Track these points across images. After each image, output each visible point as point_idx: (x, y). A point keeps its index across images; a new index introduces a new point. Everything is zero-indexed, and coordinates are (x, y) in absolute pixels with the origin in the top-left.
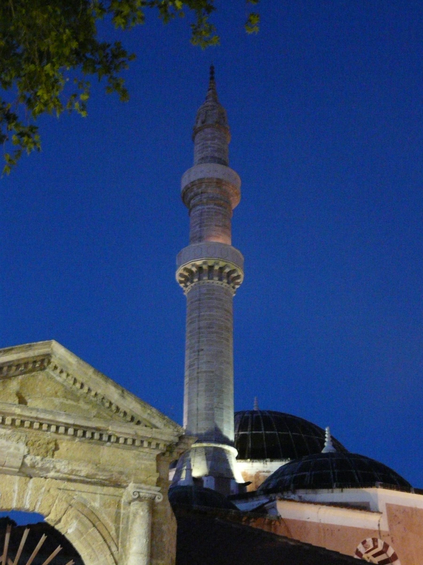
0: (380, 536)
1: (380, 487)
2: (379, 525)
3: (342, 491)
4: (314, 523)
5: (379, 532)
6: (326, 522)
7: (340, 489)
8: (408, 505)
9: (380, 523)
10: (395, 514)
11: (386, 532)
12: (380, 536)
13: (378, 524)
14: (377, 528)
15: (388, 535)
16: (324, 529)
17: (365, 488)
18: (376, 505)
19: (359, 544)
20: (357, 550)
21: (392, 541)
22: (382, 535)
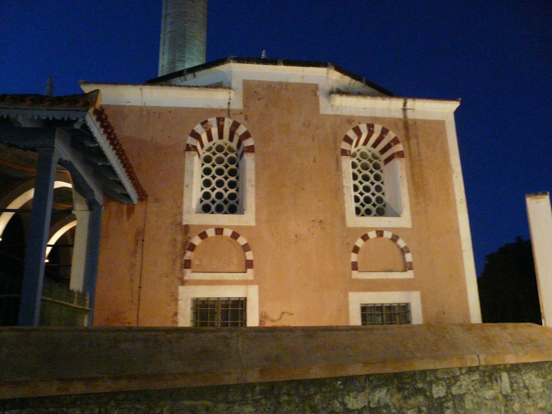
0: (229, 115)
1: (232, 61)
2: (229, 103)
3: (195, 76)
4: (136, 107)
5: (229, 111)
6: (153, 104)
7: (192, 74)
8: (277, 80)
9: (231, 101)
10: (251, 90)
11: (240, 110)
12: (229, 115)
13: (228, 102)
14: (226, 107)
15: (241, 113)
16: (148, 112)
17: (217, 66)
18: (230, 83)
19: (255, 142)
20: (193, 131)
21: (246, 119)
22: (231, 113)
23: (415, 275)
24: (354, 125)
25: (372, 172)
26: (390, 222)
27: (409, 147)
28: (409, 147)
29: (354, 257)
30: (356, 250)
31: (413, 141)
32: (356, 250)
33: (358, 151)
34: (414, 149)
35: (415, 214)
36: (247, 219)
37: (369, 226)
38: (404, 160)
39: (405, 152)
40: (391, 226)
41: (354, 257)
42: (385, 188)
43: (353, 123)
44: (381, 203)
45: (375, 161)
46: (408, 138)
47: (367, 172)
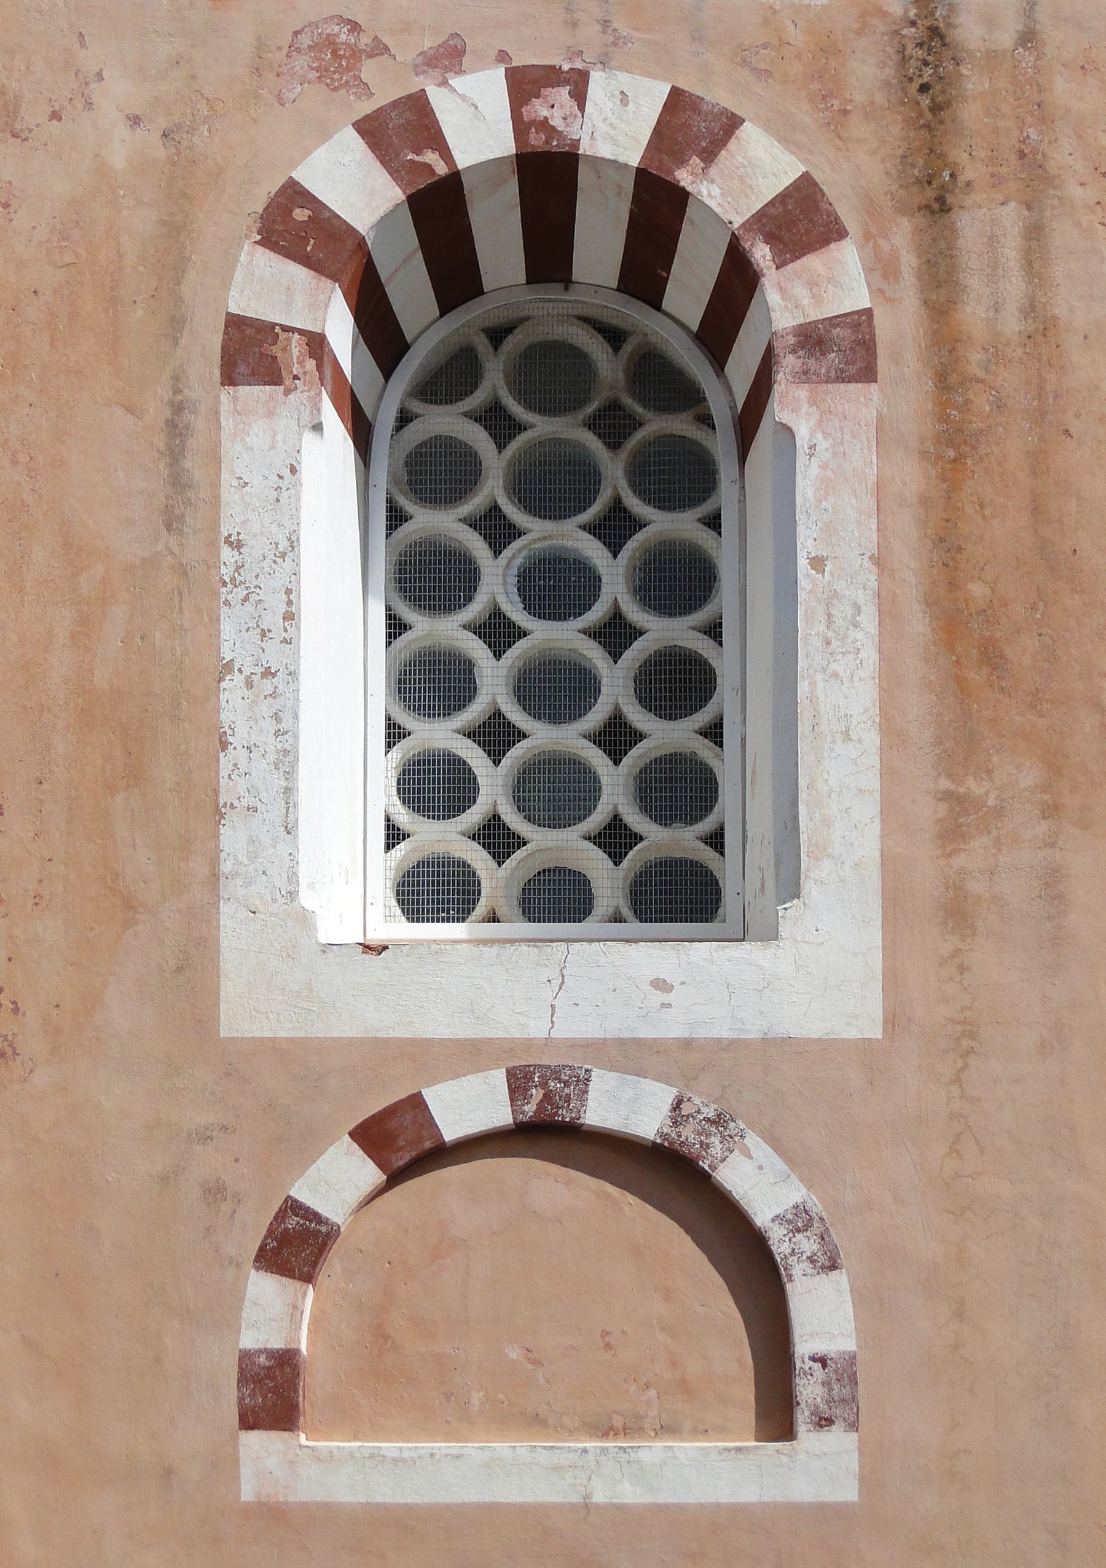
23: (870, 1481)
24: (384, 86)
25: (614, 528)
26: (660, 985)
27: (940, 279)
28: (940, 279)
29: (271, 1313)
30: (296, 1245)
31: (988, 224)
32: (296, 1245)
33: (497, 335)
34: (991, 302)
35: (932, 917)
36: (806, 968)
37: (439, 1024)
38: (862, 403)
39: (883, 328)
40: (672, 1027)
41: (271, 1313)
42: (742, 676)
43: (369, 71)
44: (691, 819)
45: (656, 425)
46: (934, 198)
47: (573, 537)
